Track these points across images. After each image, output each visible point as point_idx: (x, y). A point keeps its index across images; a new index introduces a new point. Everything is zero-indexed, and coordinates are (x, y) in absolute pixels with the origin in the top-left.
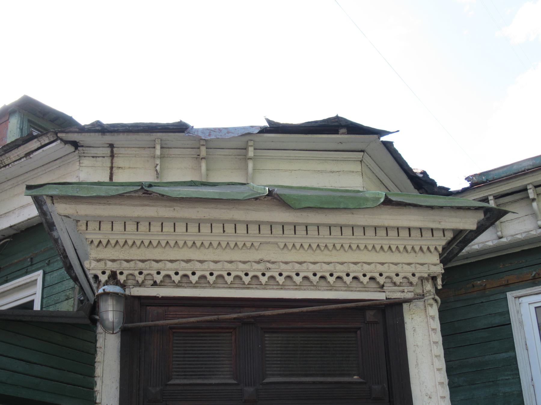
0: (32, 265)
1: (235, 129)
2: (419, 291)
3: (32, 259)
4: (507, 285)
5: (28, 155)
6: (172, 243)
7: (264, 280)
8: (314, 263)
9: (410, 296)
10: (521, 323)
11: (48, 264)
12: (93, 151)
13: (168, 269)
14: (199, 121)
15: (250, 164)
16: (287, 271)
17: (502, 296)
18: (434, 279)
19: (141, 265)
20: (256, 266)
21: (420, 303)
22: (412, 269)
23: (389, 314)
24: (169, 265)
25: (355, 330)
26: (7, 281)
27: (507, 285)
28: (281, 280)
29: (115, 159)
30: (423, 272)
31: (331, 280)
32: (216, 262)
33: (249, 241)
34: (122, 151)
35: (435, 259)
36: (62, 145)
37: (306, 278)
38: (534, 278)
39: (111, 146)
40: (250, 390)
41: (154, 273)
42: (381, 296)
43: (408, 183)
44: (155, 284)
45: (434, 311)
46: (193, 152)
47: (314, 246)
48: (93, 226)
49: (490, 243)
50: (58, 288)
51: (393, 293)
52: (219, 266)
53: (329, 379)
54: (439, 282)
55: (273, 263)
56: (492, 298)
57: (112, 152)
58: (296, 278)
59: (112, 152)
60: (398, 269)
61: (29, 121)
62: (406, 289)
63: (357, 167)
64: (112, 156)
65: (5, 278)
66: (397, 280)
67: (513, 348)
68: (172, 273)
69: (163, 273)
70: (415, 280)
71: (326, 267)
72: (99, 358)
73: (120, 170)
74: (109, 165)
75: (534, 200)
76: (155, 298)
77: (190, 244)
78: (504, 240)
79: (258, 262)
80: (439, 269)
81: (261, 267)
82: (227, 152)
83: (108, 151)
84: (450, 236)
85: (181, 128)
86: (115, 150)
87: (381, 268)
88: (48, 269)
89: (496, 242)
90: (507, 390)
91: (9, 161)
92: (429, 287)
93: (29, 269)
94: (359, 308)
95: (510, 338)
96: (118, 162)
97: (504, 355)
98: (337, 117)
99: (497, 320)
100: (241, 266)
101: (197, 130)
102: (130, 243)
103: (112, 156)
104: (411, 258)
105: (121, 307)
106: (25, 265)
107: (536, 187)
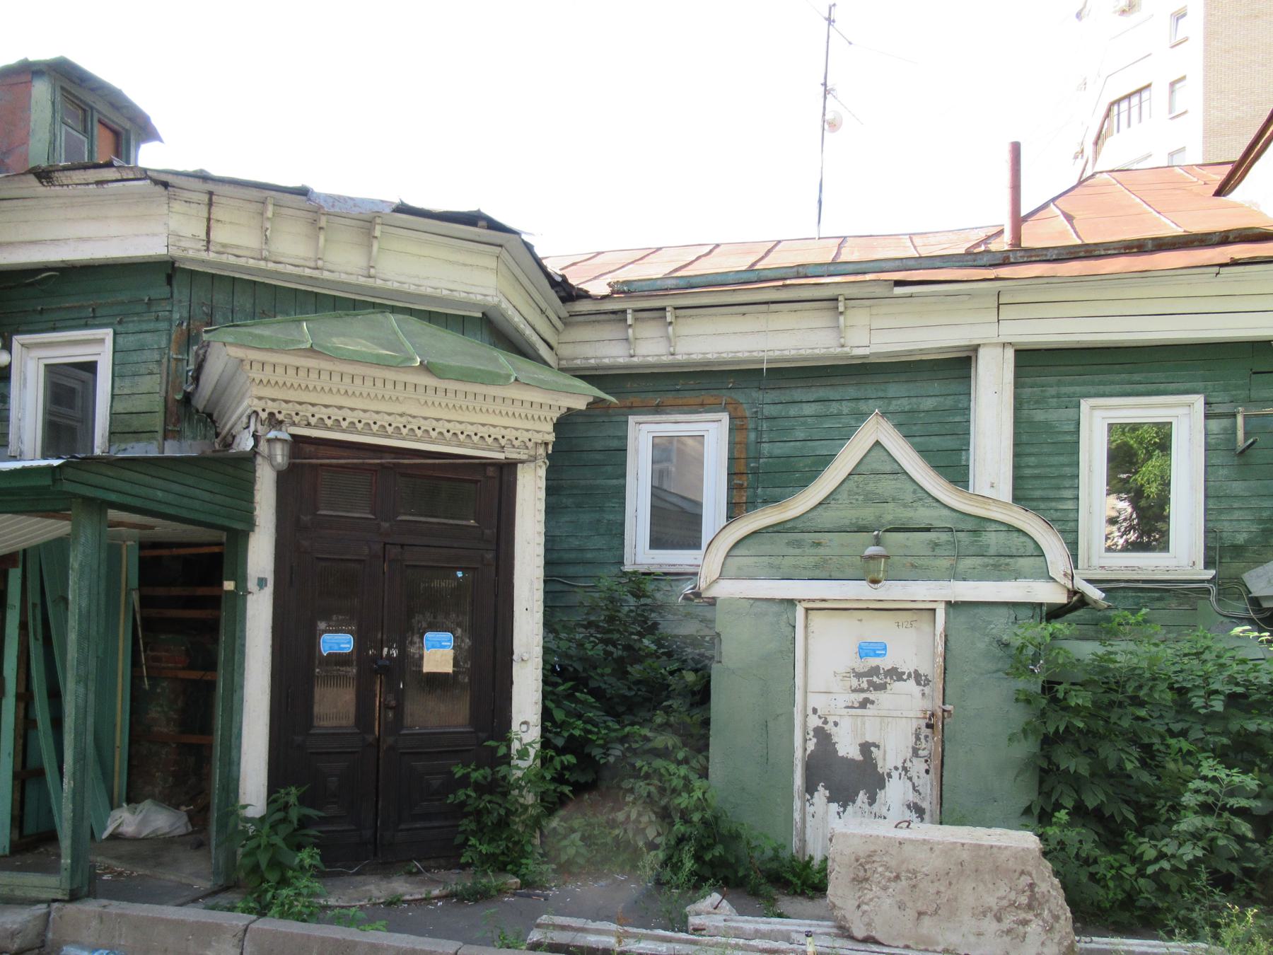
0: (94, 317)
1: (363, 201)
2: (533, 453)
3: (94, 310)
4: (631, 407)
5: (100, 183)
6: (327, 389)
7: (405, 431)
8: (449, 421)
9: (524, 457)
10: (637, 451)
11: (120, 322)
12: (187, 195)
13: (322, 413)
14: (321, 186)
15: (376, 246)
16: (426, 425)
17: (623, 419)
18: (546, 444)
19: (298, 407)
20: (399, 419)
21: (532, 465)
22: (529, 435)
23: (505, 472)
24: (323, 409)
25: (476, 482)
26: (54, 329)
27: (631, 407)
28: (419, 433)
29: (214, 209)
30: (538, 438)
31: (462, 437)
32: (365, 411)
33: (394, 395)
34: (223, 200)
35: (550, 428)
36: (152, 186)
37: (441, 433)
38: (658, 406)
39: (211, 194)
40: (386, 525)
41: (309, 415)
42: (501, 456)
43: (546, 282)
44: (309, 424)
45: (542, 472)
46: (310, 215)
47: (451, 406)
48: (256, 366)
49: (621, 360)
50: (135, 357)
51: (512, 455)
52: (367, 415)
53: (451, 522)
54: (550, 447)
55: (414, 417)
56: (614, 419)
57: (210, 200)
58: (432, 433)
59: (210, 200)
60: (518, 434)
61: (62, 88)
62: (522, 451)
63: (492, 263)
64: (210, 204)
65: (51, 325)
66: (516, 443)
67: (624, 476)
68: (325, 417)
69: (317, 416)
70: (530, 445)
71: (458, 426)
72: (257, 487)
73: (220, 225)
74: (206, 215)
75: (671, 323)
76: (309, 438)
77: (342, 391)
78: (635, 359)
79: (401, 415)
80: (551, 438)
81: (404, 420)
82: (348, 222)
83: (206, 198)
84: (564, 410)
85: (303, 192)
86: (214, 198)
87: (503, 432)
88: (119, 329)
89: (627, 360)
90: (611, 517)
91: (69, 182)
92: (541, 451)
93: (90, 322)
94: (482, 465)
95: (623, 464)
96: (217, 213)
97: (615, 482)
98: (479, 211)
99: (615, 444)
100: (387, 417)
101: (319, 195)
102: (288, 384)
103: (210, 204)
104: (529, 425)
105: (287, 448)
106: (83, 315)
107: (676, 308)
